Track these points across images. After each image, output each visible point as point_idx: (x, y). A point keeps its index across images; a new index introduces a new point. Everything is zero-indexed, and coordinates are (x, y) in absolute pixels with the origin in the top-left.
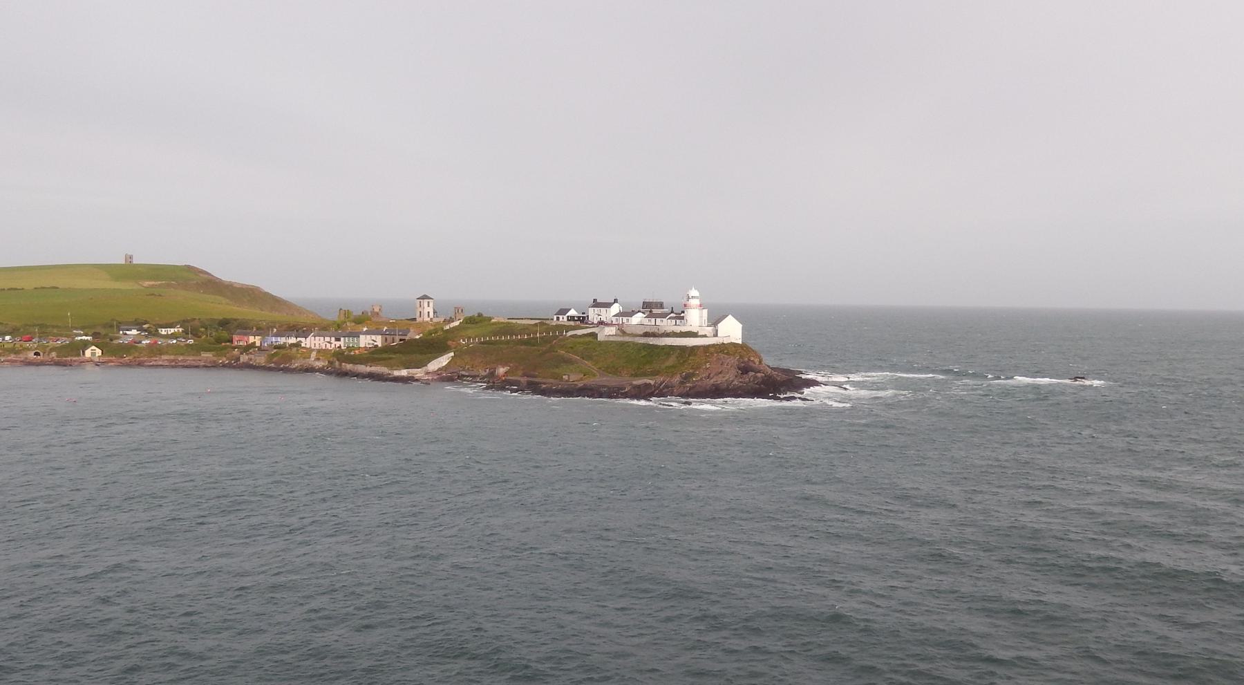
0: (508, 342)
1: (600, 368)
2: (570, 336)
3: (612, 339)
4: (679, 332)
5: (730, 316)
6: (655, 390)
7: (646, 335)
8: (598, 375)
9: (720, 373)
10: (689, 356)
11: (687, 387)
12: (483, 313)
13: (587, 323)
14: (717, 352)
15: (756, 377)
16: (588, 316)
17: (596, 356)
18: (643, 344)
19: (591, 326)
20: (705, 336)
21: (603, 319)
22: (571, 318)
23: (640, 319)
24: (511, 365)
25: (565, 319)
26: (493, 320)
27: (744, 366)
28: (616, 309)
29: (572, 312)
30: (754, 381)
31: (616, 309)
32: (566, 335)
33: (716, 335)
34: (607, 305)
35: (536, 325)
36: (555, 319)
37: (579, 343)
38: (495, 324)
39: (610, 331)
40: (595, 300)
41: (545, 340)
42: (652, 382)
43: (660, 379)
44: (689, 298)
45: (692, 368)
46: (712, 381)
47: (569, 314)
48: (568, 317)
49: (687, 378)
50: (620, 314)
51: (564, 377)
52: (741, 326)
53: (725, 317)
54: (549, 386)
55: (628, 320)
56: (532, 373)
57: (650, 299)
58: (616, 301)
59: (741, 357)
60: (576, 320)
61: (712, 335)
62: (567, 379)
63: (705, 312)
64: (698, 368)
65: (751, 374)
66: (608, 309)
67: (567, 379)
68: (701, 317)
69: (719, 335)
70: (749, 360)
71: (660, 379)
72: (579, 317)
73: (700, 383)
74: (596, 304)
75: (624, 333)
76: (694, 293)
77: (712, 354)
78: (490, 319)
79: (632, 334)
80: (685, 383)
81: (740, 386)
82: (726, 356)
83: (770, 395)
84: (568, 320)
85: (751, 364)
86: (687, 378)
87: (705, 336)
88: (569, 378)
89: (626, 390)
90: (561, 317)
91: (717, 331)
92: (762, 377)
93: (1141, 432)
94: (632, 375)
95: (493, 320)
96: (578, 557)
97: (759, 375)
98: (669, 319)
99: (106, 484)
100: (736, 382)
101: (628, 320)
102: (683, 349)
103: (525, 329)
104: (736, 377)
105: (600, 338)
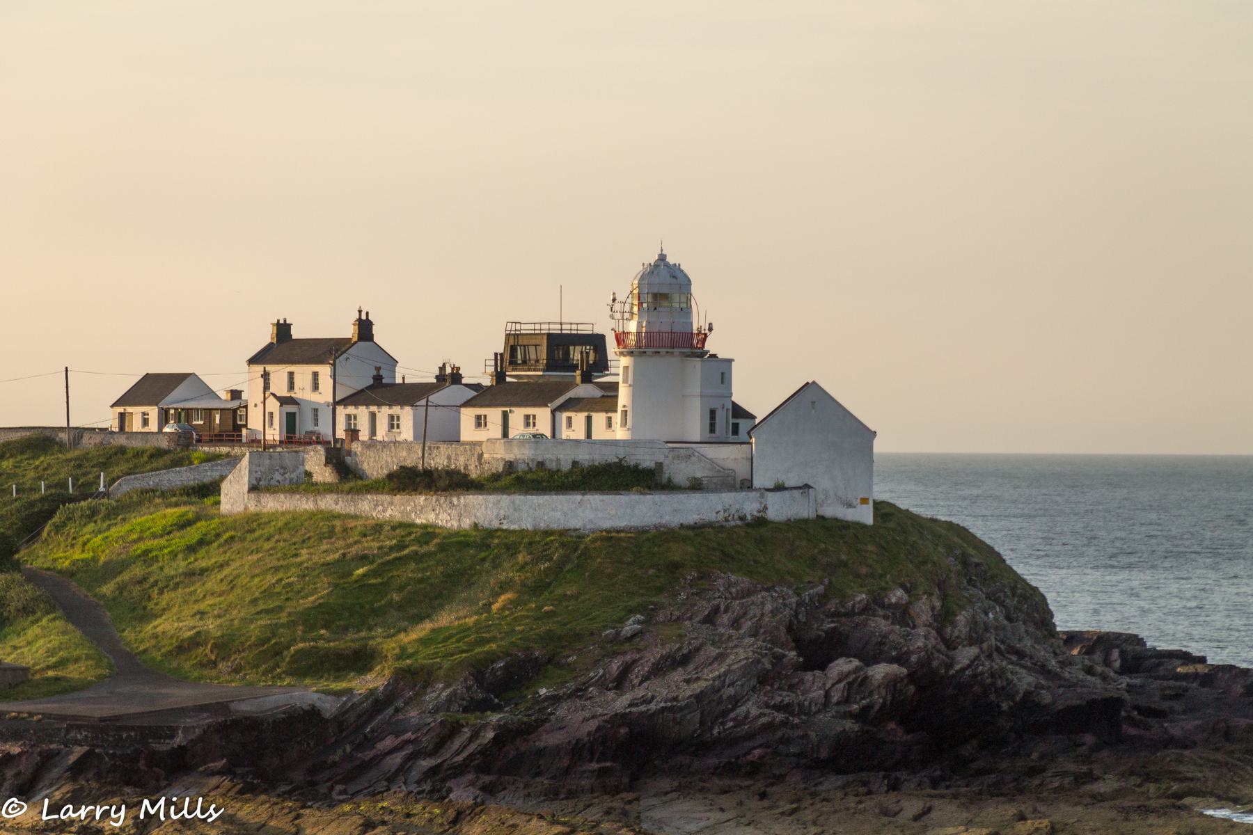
4: (566, 467)
30: (846, 700)
40: (283, 329)
65: (842, 666)
97: (880, 671)
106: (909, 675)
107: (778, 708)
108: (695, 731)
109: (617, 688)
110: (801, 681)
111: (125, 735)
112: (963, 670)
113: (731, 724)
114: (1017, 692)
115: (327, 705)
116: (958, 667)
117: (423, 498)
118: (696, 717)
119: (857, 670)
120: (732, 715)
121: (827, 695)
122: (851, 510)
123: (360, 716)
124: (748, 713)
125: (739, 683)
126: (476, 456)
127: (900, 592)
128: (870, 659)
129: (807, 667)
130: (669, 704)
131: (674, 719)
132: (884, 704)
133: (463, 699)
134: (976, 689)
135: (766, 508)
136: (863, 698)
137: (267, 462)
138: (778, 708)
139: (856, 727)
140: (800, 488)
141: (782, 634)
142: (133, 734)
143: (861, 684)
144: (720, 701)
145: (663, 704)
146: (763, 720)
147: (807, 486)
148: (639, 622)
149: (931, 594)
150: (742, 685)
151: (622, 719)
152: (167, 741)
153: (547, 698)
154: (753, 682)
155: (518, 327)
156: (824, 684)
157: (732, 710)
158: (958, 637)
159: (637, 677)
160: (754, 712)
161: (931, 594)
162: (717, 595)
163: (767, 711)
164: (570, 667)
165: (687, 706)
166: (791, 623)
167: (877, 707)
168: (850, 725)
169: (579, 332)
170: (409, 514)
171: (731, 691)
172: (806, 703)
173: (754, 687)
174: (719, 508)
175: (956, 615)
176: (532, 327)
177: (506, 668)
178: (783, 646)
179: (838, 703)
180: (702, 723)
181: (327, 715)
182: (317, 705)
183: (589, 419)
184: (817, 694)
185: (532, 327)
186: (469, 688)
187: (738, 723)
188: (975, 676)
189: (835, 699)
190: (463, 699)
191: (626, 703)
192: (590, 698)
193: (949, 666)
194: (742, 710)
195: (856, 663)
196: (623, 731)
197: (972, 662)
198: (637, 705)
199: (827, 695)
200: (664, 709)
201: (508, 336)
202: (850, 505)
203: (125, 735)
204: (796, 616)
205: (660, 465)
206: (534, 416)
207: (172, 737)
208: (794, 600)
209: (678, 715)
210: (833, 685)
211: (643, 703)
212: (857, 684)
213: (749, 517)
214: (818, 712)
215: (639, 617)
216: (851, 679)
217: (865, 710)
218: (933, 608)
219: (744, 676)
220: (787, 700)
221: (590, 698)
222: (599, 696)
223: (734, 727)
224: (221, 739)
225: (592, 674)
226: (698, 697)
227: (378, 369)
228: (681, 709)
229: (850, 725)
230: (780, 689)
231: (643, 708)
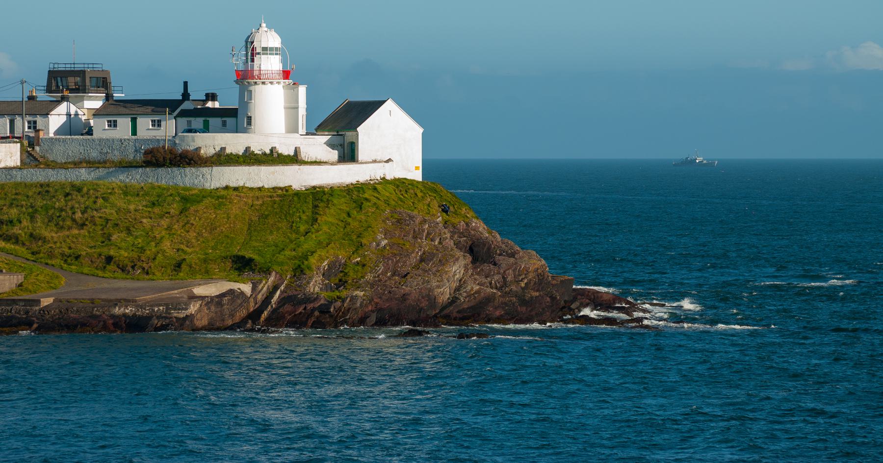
3: (19, 177)
33: (348, 154)
52: (421, 130)
63: (302, 90)
68: (292, 108)
100: (473, 287)
108: (448, 299)
110: (482, 270)
111: (156, 309)
118: (316, 296)
125: (458, 271)
142: (161, 308)
150: (459, 272)
152: (183, 311)
169: (59, 69)
176: (64, 66)
202: (409, 171)
203: (156, 309)
207: (186, 309)
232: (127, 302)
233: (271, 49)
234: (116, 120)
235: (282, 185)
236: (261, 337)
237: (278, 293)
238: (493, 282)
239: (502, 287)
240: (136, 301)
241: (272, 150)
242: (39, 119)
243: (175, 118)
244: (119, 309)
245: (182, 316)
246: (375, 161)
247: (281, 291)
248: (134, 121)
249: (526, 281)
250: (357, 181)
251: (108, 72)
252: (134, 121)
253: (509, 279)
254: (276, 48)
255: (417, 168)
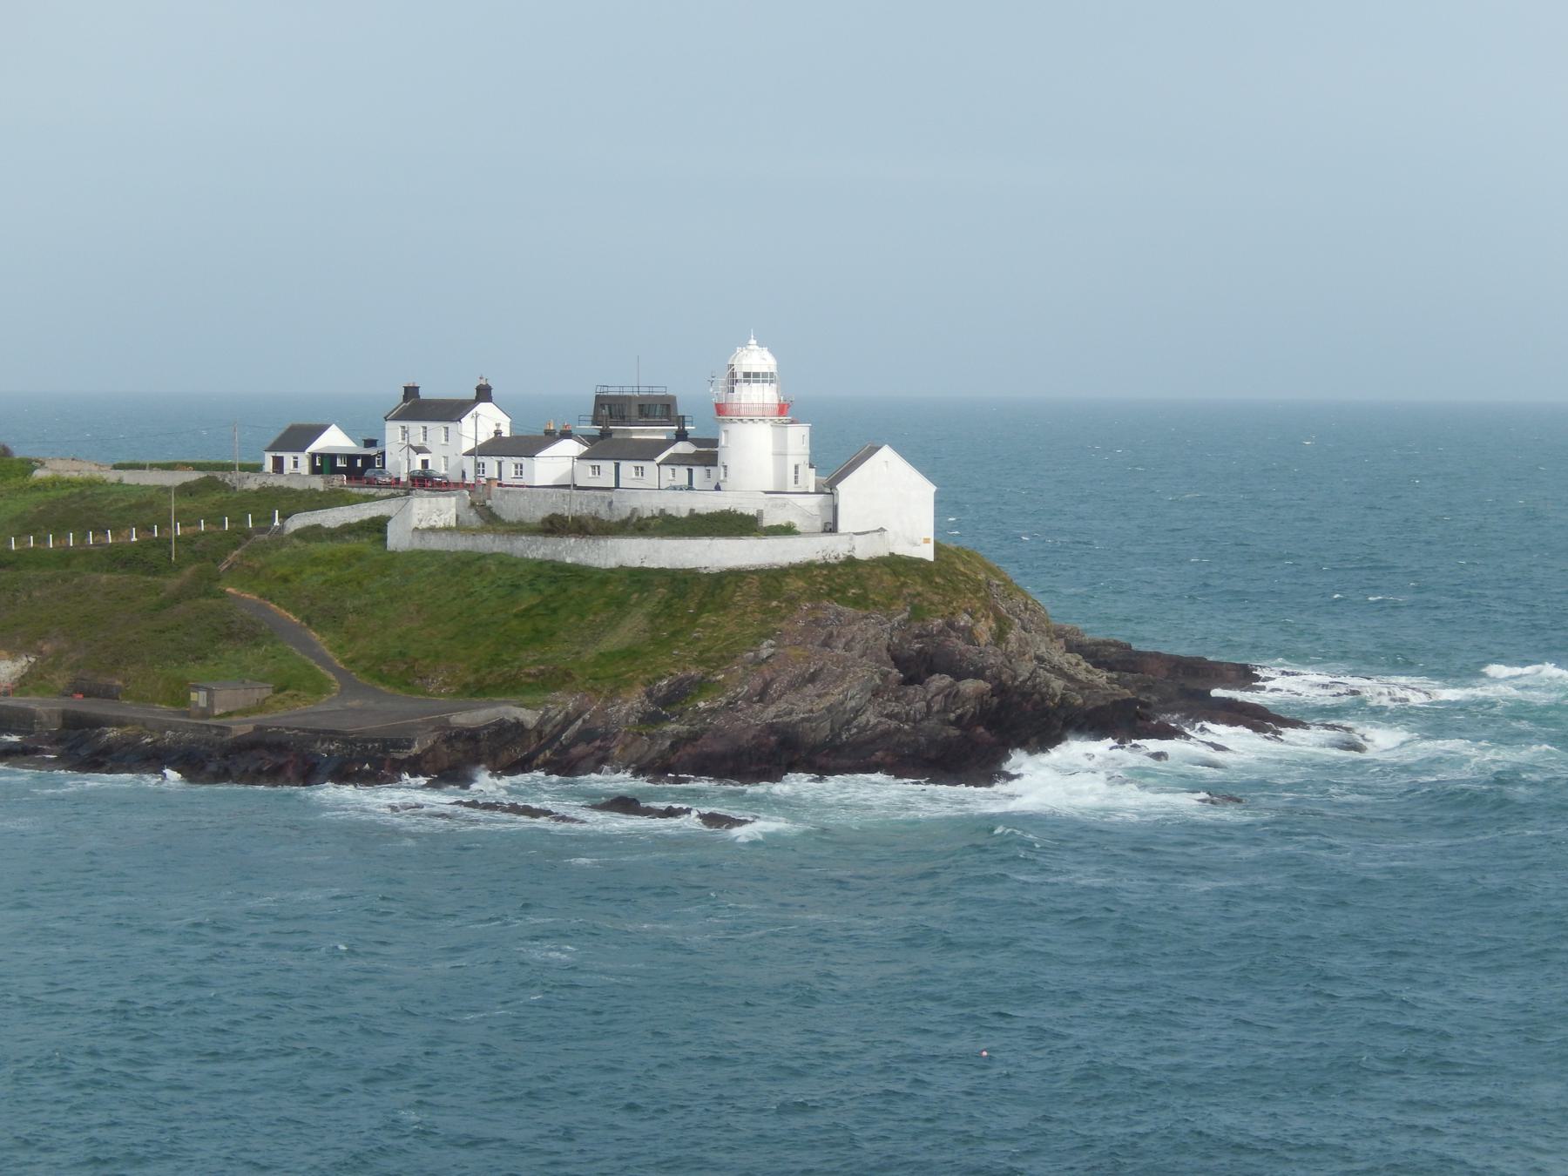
0: (65, 558)
1: (353, 661)
2: (299, 534)
3: (435, 543)
4: (684, 514)
5: (886, 453)
6: (541, 749)
7: (555, 526)
8: (336, 686)
9: (812, 678)
10: (701, 608)
11: (663, 735)
12: (13, 448)
13: (371, 483)
14: (815, 596)
15: (952, 696)
16: (383, 453)
17: (356, 611)
18: (541, 563)
19: (385, 492)
20: (787, 530)
21: (438, 467)
22: (325, 464)
23: (567, 466)
24: (46, 648)
25: (304, 467)
26: (39, 474)
27: (920, 651)
28: (487, 421)
29: (334, 440)
30: (945, 710)
31: (487, 421)
32: (282, 527)
33: (831, 528)
34: (451, 411)
35: (186, 490)
36: (269, 465)
37: (315, 561)
38: (39, 487)
39: (434, 511)
40: (411, 392)
41: (206, 552)
42: (530, 718)
43: (563, 703)
44: (733, 380)
45: (699, 661)
46: (770, 714)
47: (321, 444)
48: (313, 456)
49: (677, 697)
50: (496, 447)
51: (194, 696)
52: (933, 489)
53: (874, 450)
54: (129, 730)
55: (519, 467)
56: (103, 680)
57: (626, 381)
58: (484, 394)
59: (917, 613)
60: (340, 471)
61: (819, 525)
62: (203, 704)
64: (727, 658)
65: (940, 681)
66: (451, 426)
67: (203, 704)
68: (781, 454)
69: (842, 527)
70: (951, 625)
71: (563, 703)
72: (351, 459)
73: (720, 721)
74: (415, 407)
75: (490, 519)
76: (756, 358)
77: (792, 601)
78: (28, 466)
79: (521, 523)
80: (666, 719)
81: (886, 734)
82: (849, 611)
83: (670, 775)
84: (315, 470)
85: (958, 644)
86: (677, 697)
87: (787, 530)
88: (211, 704)
89: (416, 749)
90: (288, 458)
91: (835, 509)
92: (980, 696)
93: (1506, 623)
94: (466, 686)
95: (39, 474)
96: (1121, 1138)
97: (969, 686)
98: (666, 462)
99: (594, 934)
100: (870, 717)
101: (519, 467)
102: (681, 581)
103: (145, 506)
104: (876, 693)
105: (398, 538)
106: (992, 690)
107: (889, 716)
108: (827, 736)
109: (760, 701)
110: (906, 694)
111: (370, 746)
112: (1025, 682)
113: (855, 730)
114: (1056, 695)
115: (528, 718)
116: (1020, 679)
117: (573, 540)
118: (828, 725)
119: (951, 685)
120: (855, 723)
121: (929, 706)
122: (916, 548)
123: (555, 726)
124: (868, 721)
126: (606, 504)
127: (966, 617)
128: (959, 676)
129: (909, 681)
130: (807, 715)
131: (811, 727)
132: (974, 713)
133: (638, 712)
134: (1036, 697)
135: (854, 548)
136: (958, 708)
137: (427, 506)
138: (889, 716)
139: (957, 732)
140: (878, 531)
141: (885, 656)
143: (955, 696)
144: (845, 712)
145: (802, 715)
146: (881, 727)
147: (882, 530)
148: (772, 646)
149: (987, 617)
151: (771, 728)
153: (705, 711)
154: (869, 695)
155: (605, 389)
156: (925, 697)
157: (855, 718)
158: (1012, 652)
159: (775, 692)
160: (873, 721)
161: (987, 617)
162: (829, 623)
163: (883, 720)
164: (722, 686)
165: (821, 716)
166: (889, 645)
167: (968, 716)
168: (954, 732)
170: (560, 552)
171: (853, 703)
172: (912, 712)
173: (870, 700)
174: (818, 549)
175: (1007, 634)
176: (647, 389)
177: (669, 685)
178: (885, 664)
179: (938, 712)
180: (832, 730)
181: (530, 726)
182: (521, 717)
183: (690, 471)
184: (921, 705)
185: (647, 389)
186: (642, 703)
187: (862, 729)
188: (1034, 686)
189: (935, 709)
190: (638, 712)
191: (772, 715)
192: (741, 710)
193: (1014, 678)
194: (862, 719)
195: (948, 680)
196: (773, 738)
197: (1031, 674)
198: (780, 716)
199: (929, 706)
200: (803, 720)
201: (597, 397)
202: (915, 544)
203: (370, 746)
204: (891, 639)
205: (760, 512)
206: (642, 468)
208: (888, 625)
209: (814, 724)
210: (933, 697)
211: (786, 714)
212: (952, 696)
213: (841, 556)
214: (922, 719)
215: (770, 641)
216: (946, 692)
217: (960, 717)
218: (990, 629)
219: (862, 690)
220: (896, 710)
221: (741, 710)
222: (747, 708)
223: (858, 733)
224: (448, 748)
225: (739, 690)
226: (829, 709)
227: (498, 425)
228: (816, 719)
229: (954, 732)
230: (889, 700)
231: (786, 719)
232: (331, 735)
233: (756, 375)
234: (282, 458)
235: (688, 566)
236: (1484, 756)
237: (580, 722)
238: (912, 712)
239: (922, 719)
240: (344, 734)
241: (632, 514)
242: (524, 461)
243: (658, 465)
244: (322, 744)
245: (402, 756)
246: (868, 532)
247: (584, 721)
248: (690, 471)
249: (959, 711)
250: (891, 554)
251: (673, 399)
252: (617, 467)
253: (935, 709)
254: (765, 375)
255: (927, 541)
